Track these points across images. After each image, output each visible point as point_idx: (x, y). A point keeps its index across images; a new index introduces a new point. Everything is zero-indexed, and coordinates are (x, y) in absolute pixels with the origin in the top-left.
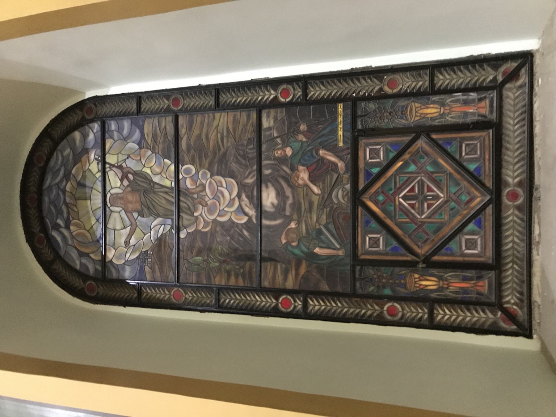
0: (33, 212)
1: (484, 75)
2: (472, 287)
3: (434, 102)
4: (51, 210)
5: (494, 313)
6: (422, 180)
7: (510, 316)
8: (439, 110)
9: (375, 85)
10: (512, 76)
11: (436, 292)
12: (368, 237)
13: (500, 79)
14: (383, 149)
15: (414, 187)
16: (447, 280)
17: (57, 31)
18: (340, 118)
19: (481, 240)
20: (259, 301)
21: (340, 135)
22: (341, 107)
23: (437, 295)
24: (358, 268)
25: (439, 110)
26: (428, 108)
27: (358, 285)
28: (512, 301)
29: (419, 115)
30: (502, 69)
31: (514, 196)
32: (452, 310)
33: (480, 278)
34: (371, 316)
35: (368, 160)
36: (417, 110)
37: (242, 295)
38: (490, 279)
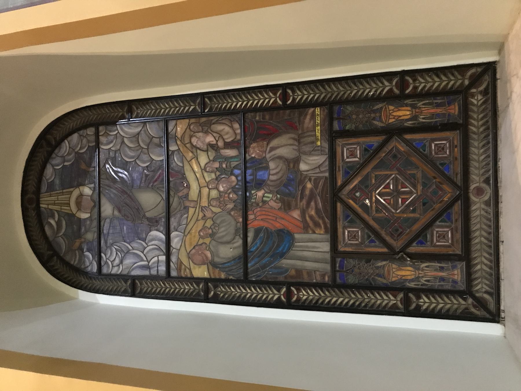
0: (32, 213)
1: (68, 125)
2: (447, 275)
3: (407, 105)
4: (402, 202)
5: (465, 299)
6: (397, 177)
7: (481, 303)
8: (411, 113)
9: (378, 87)
10: (475, 81)
11: (413, 282)
12: (347, 230)
13: (467, 82)
14: (360, 148)
15: (389, 183)
16: (423, 270)
17: (183, 22)
18: (318, 120)
19: (361, 232)
20: (168, 288)
21: (318, 136)
22: (318, 110)
23: (415, 285)
24: (338, 260)
25: (411, 113)
26: (399, 110)
27: (338, 275)
28: (484, 290)
29: (393, 117)
30: (469, 73)
31: (480, 191)
32: (241, 288)
33: (454, 267)
34: (449, 310)
35: (346, 159)
36: (391, 112)
37: (314, 290)
38: (462, 268)
